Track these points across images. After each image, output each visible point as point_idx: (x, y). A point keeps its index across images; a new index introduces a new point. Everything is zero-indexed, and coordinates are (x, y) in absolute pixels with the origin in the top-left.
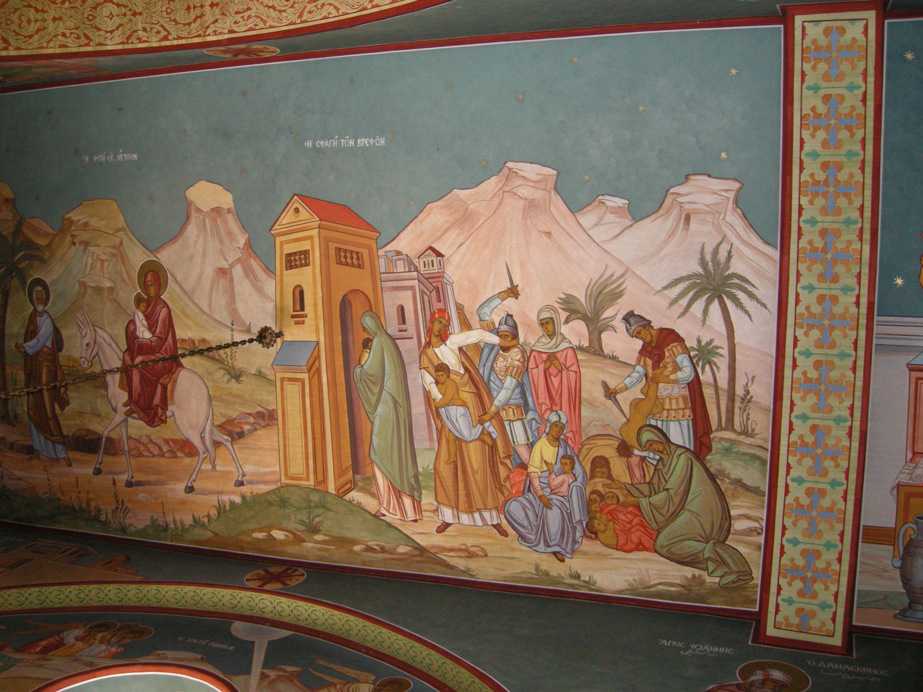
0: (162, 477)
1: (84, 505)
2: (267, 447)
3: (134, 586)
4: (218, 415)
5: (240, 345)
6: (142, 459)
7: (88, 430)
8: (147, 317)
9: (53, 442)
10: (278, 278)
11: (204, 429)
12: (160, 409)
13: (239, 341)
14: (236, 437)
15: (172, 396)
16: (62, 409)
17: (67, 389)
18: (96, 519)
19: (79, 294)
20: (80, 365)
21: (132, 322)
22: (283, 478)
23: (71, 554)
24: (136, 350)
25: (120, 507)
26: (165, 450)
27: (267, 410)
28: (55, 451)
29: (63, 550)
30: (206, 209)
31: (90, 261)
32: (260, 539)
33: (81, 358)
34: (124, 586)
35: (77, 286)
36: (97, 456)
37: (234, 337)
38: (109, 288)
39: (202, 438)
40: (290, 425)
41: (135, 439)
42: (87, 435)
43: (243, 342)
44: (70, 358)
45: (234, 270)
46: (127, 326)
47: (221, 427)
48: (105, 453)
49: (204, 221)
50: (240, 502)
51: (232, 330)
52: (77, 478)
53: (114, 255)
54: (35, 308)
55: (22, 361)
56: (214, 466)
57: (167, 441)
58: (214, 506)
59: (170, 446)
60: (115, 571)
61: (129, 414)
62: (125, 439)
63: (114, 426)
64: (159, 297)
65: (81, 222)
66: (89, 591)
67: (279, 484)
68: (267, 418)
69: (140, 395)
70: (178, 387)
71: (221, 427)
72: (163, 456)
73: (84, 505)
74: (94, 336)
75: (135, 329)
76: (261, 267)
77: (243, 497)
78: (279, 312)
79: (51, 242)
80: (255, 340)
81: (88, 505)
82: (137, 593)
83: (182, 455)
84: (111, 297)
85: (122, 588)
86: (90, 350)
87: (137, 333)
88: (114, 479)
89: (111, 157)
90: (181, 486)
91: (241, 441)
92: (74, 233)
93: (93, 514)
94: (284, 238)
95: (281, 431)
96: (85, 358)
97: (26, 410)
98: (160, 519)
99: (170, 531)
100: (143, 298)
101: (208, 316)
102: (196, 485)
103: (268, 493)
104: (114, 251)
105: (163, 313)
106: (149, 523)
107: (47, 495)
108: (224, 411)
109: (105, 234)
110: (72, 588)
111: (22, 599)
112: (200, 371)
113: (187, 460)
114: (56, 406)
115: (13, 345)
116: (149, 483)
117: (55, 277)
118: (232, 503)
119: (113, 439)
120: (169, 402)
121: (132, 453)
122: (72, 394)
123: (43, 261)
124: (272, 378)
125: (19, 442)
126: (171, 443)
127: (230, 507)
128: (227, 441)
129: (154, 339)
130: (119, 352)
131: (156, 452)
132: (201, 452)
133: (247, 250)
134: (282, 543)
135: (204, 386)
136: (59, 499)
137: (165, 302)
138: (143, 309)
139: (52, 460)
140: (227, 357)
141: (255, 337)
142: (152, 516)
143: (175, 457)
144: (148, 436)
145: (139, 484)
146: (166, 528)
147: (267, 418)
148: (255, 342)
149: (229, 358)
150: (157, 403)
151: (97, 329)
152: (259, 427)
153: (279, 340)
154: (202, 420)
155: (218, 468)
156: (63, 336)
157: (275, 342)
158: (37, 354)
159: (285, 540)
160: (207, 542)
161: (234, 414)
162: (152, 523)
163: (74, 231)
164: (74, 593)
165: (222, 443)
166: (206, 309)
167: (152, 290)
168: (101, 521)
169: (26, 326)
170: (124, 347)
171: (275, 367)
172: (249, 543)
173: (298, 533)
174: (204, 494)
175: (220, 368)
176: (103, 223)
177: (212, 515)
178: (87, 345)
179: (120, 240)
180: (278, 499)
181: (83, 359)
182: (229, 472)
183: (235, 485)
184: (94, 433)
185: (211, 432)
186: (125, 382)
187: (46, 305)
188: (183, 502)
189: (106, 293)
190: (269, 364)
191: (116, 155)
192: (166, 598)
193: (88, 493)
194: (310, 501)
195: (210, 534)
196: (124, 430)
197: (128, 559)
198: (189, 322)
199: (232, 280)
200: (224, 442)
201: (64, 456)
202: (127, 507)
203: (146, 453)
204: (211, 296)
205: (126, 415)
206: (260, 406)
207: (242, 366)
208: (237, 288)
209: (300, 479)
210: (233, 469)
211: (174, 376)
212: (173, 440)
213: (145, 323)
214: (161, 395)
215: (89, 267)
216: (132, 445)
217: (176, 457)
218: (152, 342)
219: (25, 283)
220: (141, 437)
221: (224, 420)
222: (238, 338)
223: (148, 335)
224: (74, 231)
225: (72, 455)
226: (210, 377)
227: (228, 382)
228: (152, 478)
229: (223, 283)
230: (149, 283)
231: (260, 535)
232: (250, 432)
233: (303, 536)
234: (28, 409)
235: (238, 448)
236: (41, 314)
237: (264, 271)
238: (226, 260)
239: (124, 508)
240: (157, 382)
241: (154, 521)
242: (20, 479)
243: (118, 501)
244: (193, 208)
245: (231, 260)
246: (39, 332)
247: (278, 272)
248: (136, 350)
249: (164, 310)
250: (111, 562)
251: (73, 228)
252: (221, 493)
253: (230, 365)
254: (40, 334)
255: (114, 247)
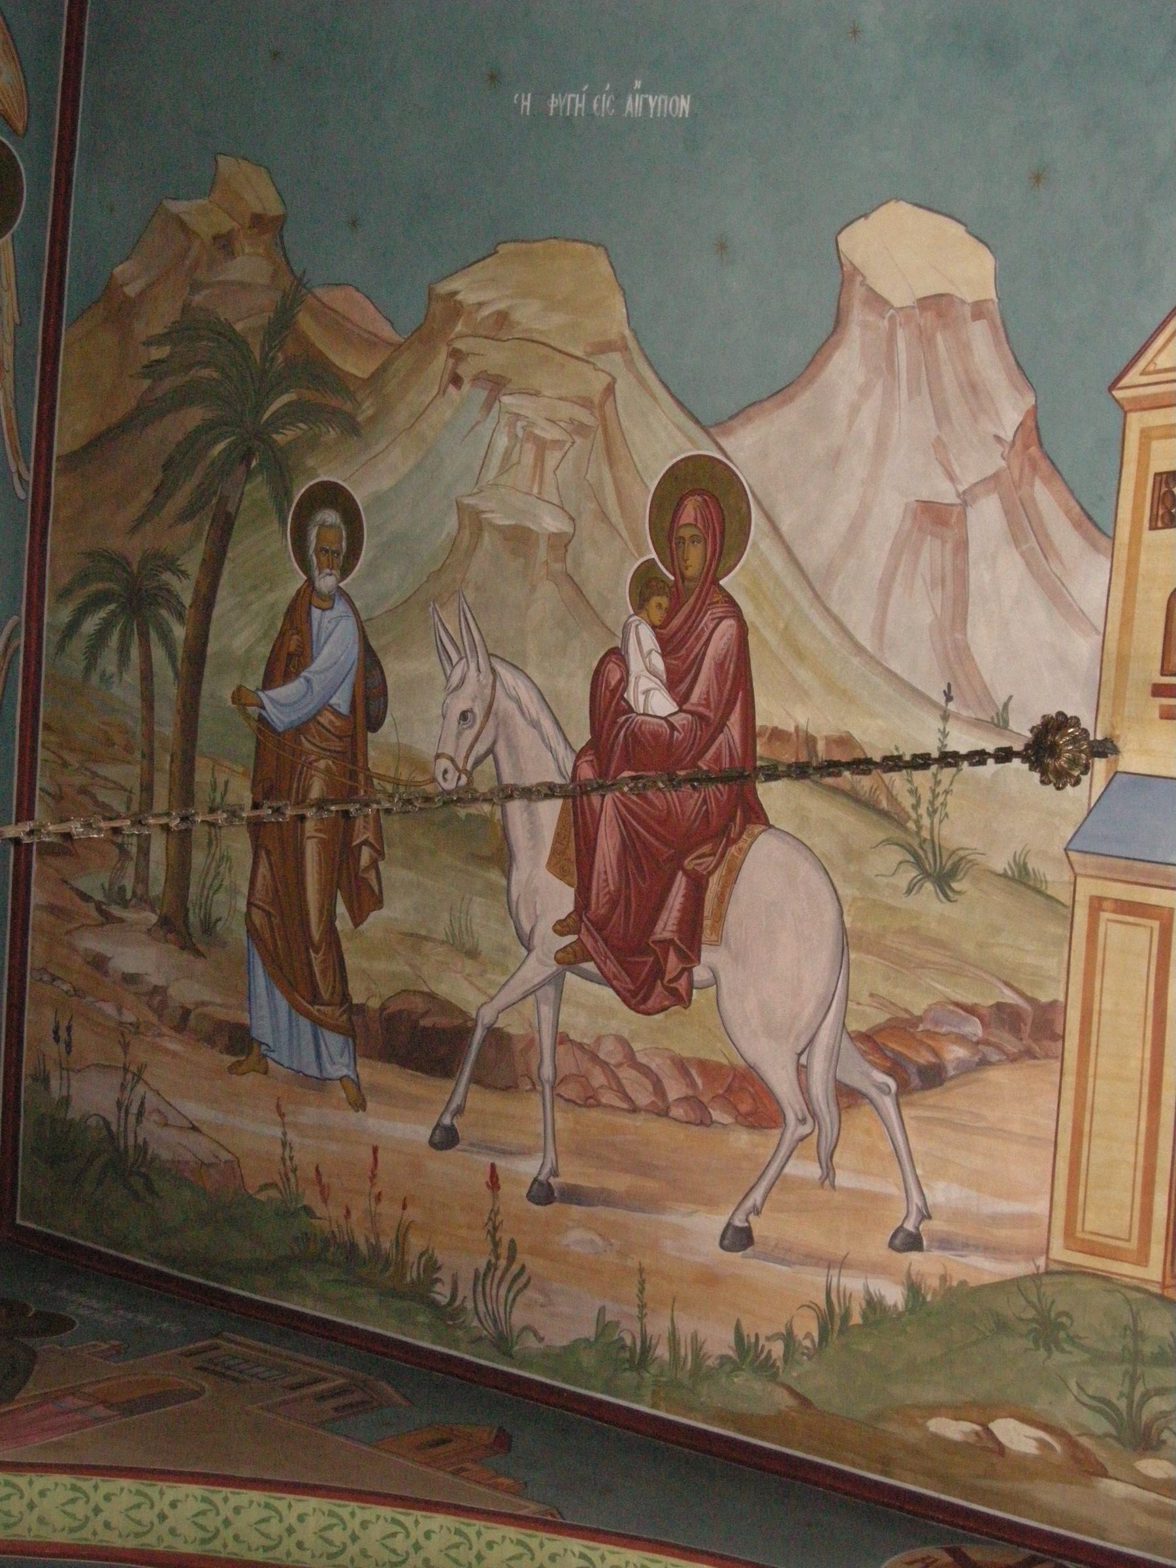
0: (651, 1185)
1: (387, 1244)
2: (1016, 1127)
3: (512, 1532)
4: (865, 999)
5: (965, 765)
6: (595, 1114)
7: (432, 996)
8: (668, 646)
9: (317, 1023)
10: (1122, 553)
11: (811, 1041)
12: (672, 957)
13: (963, 750)
14: (915, 1081)
15: (720, 917)
16: (358, 918)
17: (381, 854)
18: (420, 1293)
19: (455, 543)
20: (433, 780)
21: (617, 655)
22: (1057, 1242)
23: (321, 1397)
24: (618, 751)
25: (503, 1262)
26: (672, 1095)
27: (1031, 1001)
28: (318, 1056)
29: (298, 1379)
30: (900, 296)
31: (502, 442)
32: (956, 1443)
33: (438, 756)
34: (479, 1524)
35: (452, 522)
36: (449, 1084)
37: (948, 741)
38: (552, 536)
39: (802, 1071)
40: (1104, 1062)
41: (581, 1046)
42: (425, 1014)
43: (978, 757)
44: (404, 755)
45: (971, 514)
46: (598, 673)
47: (869, 1041)
48: (475, 1079)
49: (891, 338)
50: (901, 1306)
51: (945, 717)
52: (375, 1150)
53: (581, 429)
54: (310, 581)
55: (248, 747)
56: (829, 1171)
57: (681, 1066)
58: (811, 1306)
59: (693, 1084)
60: (455, 1473)
61: (569, 959)
62: (547, 1042)
63: (519, 992)
64: (715, 582)
65: (486, 312)
66: (237, 1510)
67: (1041, 1262)
68: (1027, 1029)
69: (613, 903)
70: (742, 888)
71: (869, 1041)
72: (664, 1113)
73: (387, 1244)
74: (488, 691)
75: (624, 680)
76: (1067, 513)
77: (914, 1289)
78: (1110, 673)
79: (383, 369)
80: (1018, 754)
81: (400, 1243)
82: (203, 1513)
83: (727, 1119)
84: (558, 566)
85: (217, 1498)
86: (469, 735)
87: (630, 695)
88: (493, 1166)
89: (606, 102)
90: (712, 1223)
91: (932, 1096)
92: (460, 345)
93: (412, 1274)
94: (1156, 418)
95: (1070, 1080)
96: (452, 760)
97: (242, 905)
98: (625, 1324)
99: (653, 1369)
100: (664, 580)
101: (874, 661)
102: (759, 1227)
103: (1000, 1287)
104: (583, 415)
105: (723, 634)
106: (588, 1331)
107: (273, 1193)
108: (883, 989)
109: (558, 357)
110: (311, 1503)
111: (147, 1515)
112: (821, 843)
113: (743, 1139)
114: (341, 908)
115: (227, 694)
116: (605, 1198)
117: (387, 483)
118: (873, 1305)
119: (509, 1037)
120: (707, 935)
121: (562, 1090)
122: (393, 874)
123: (352, 428)
124: (1065, 897)
125: (209, 1010)
126: (694, 1072)
127: (864, 1316)
128: (884, 1090)
129: (680, 720)
130: (561, 750)
131: (643, 1098)
132: (791, 1118)
133: (1026, 447)
134: (1023, 1466)
135: (826, 895)
136: (308, 1210)
137: (731, 601)
138: (657, 616)
139: (302, 1078)
140: (915, 807)
141: (1018, 747)
142: (602, 1310)
143: (701, 1123)
144: (624, 1043)
145: (573, 1195)
146: (642, 1358)
147: (1027, 1029)
148: (1016, 762)
149: (923, 810)
150: (667, 935)
151: (501, 669)
152: (995, 1057)
153: (1099, 765)
154: (809, 1009)
155: (843, 1179)
156: (390, 682)
157: (1086, 769)
158: (300, 729)
159: (1036, 1458)
160: (775, 1423)
161: (918, 1004)
162: (597, 1337)
163: (461, 336)
164: (313, 1523)
165: (864, 1096)
166: (864, 637)
167: (694, 558)
168: (434, 1304)
169: (275, 634)
170: (581, 736)
171: (1074, 856)
172: (915, 1451)
173: (1084, 1441)
174: (782, 1261)
175: (888, 841)
176: (558, 319)
177: (799, 1334)
178: (464, 716)
179: (605, 380)
180: (1030, 1314)
181: (444, 763)
182: (875, 1197)
183: (891, 1245)
184: (447, 1007)
185: (835, 1057)
186: (572, 852)
187: (345, 572)
188: (710, 1278)
189: (542, 553)
190: (1057, 849)
191: (619, 98)
192: (169, 1523)
193: (404, 1207)
194: (1138, 1335)
195: (784, 1400)
196: (546, 1011)
197: (503, 1442)
198: (804, 675)
199: (962, 546)
200: (873, 1093)
201: (345, 1072)
202: (523, 1268)
203: (608, 1098)
204: (886, 589)
205: (558, 961)
206: (1007, 984)
207: (965, 841)
208: (979, 575)
209: (1113, 1254)
210: (893, 1189)
211: (733, 850)
212: (703, 1065)
213: (658, 663)
214: (684, 910)
215: (495, 462)
216: (568, 1066)
217: (705, 1121)
218: (672, 727)
219: (288, 494)
220: (599, 1040)
221: (880, 1017)
222: (962, 741)
223: (662, 704)
224: (461, 336)
225: (372, 1072)
226: (853, 868)
227: (909, 891)
228: (618, 1182)
229: (933, 554)
230: (687, 533)
231: (954, 1429)
232: (967, 1069)
233: (1102, 1455)
234: (250, 904)
235: (917, 1119)
236: (328, 602)
237: (1077, 526)
238: (952, 478)
239: (515, 1268)
240: (677, 863)
241: (604, 1327)
242: (194, 1128)
243: (496, 1244)
244: (858, 292)
245: (968, 479)
246: (312, 660)
247: (1124, 532)
248: (618, 751)
249: (728, 627)
250: (444, 1442)
251: (459, 328)
252: (842, 1264)
253: (925, 834)
254: (314, 667)
255: (585, 403)
